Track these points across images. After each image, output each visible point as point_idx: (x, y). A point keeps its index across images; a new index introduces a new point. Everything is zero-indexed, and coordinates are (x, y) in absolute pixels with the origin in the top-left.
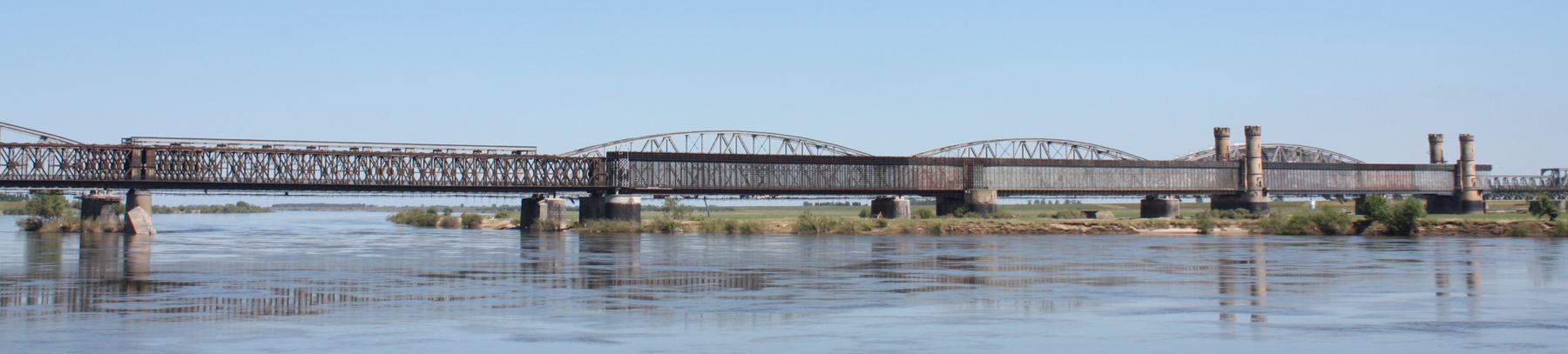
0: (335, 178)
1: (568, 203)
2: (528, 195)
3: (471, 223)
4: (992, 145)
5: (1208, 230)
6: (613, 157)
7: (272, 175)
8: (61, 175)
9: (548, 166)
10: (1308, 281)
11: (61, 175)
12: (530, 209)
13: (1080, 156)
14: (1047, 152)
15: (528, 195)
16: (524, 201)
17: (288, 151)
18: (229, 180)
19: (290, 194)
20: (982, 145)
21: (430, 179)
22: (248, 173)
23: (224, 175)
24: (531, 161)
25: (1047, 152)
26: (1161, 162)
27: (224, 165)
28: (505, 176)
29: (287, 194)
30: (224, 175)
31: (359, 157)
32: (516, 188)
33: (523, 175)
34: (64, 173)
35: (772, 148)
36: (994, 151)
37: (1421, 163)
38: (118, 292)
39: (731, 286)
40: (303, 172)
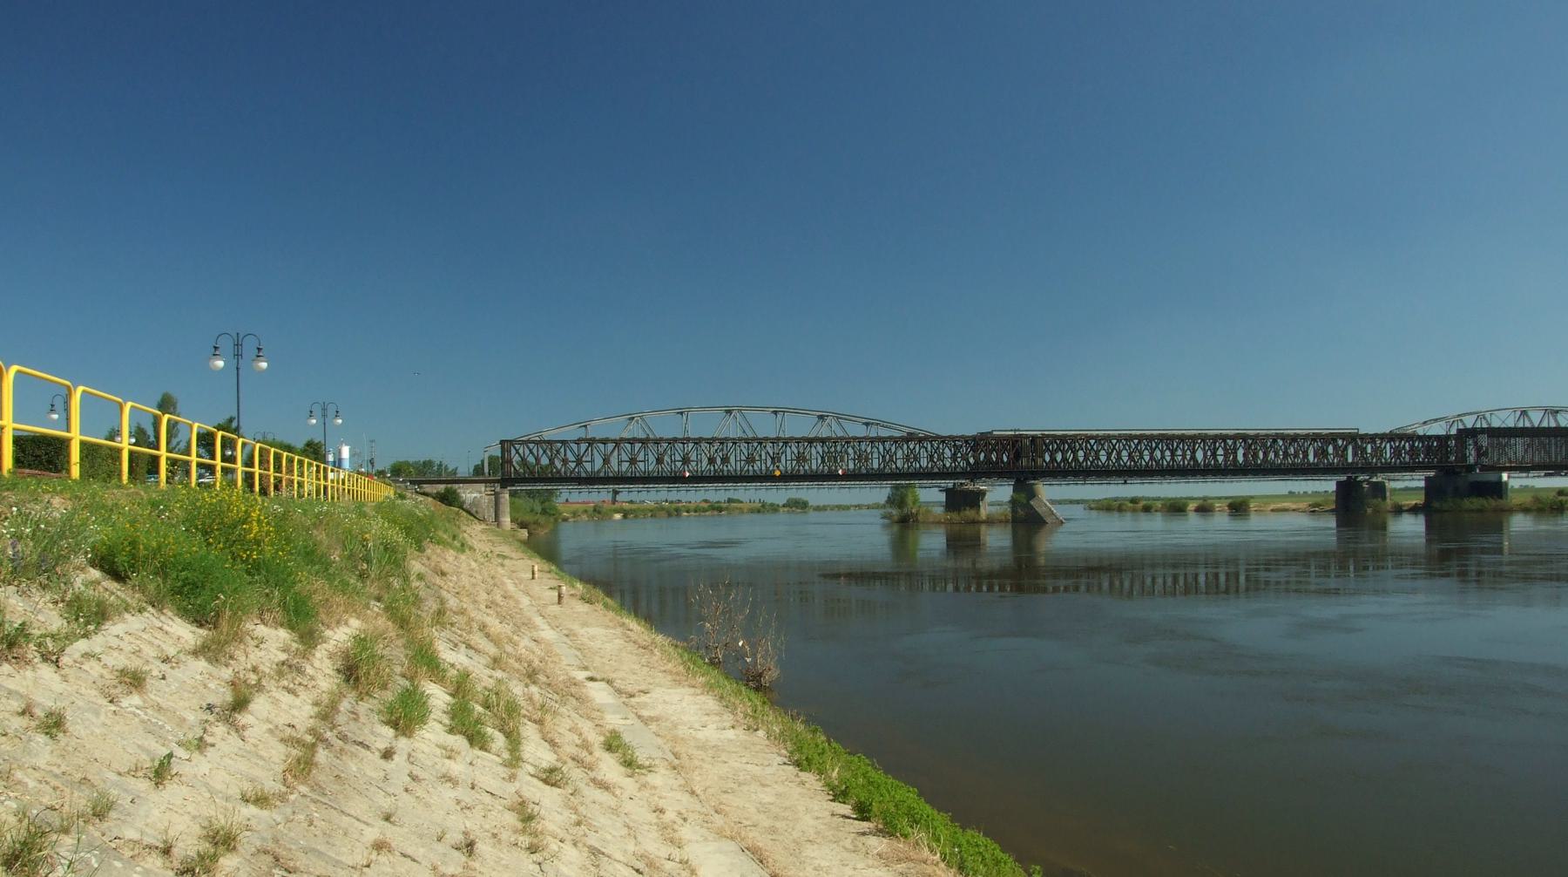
0: (918, 465)
1: (1409, 485)
2: (1343, 478)
3: (1204, 509)
4: (1488, 415)
5: (425, 543)
6: (1466, 434)
7: (876, 466)
8: (748, 470)
9: (513, 451)
10: (1535, 557)
11: (748, 470)
12: (897, 500)
13: (1464, 424)
14: (1556, 420)
15: (1343, 478)
16: (1339, 484)
17: (890, 438)
18: (819, 472)
19: (1128, 482)
20: (1476, 416)
21: (961, 464)
22: (734, 465)
23: (814, 467)
24: (1092, 442)
25: (1556, 420)
26: (979, 442)
27: (875, 455)
28: (1193, 458)
29: (1125, 483)
30: (814, 467)
31: (920, 442)
32: (1328, 470)
33: (1218, 453)
34: (751, 468)
35: (814, 424)
36: (1489, 420)
37: (1435, 434)
38: (1333, 571)
39: (1309, 572)
40: (908, 461)
